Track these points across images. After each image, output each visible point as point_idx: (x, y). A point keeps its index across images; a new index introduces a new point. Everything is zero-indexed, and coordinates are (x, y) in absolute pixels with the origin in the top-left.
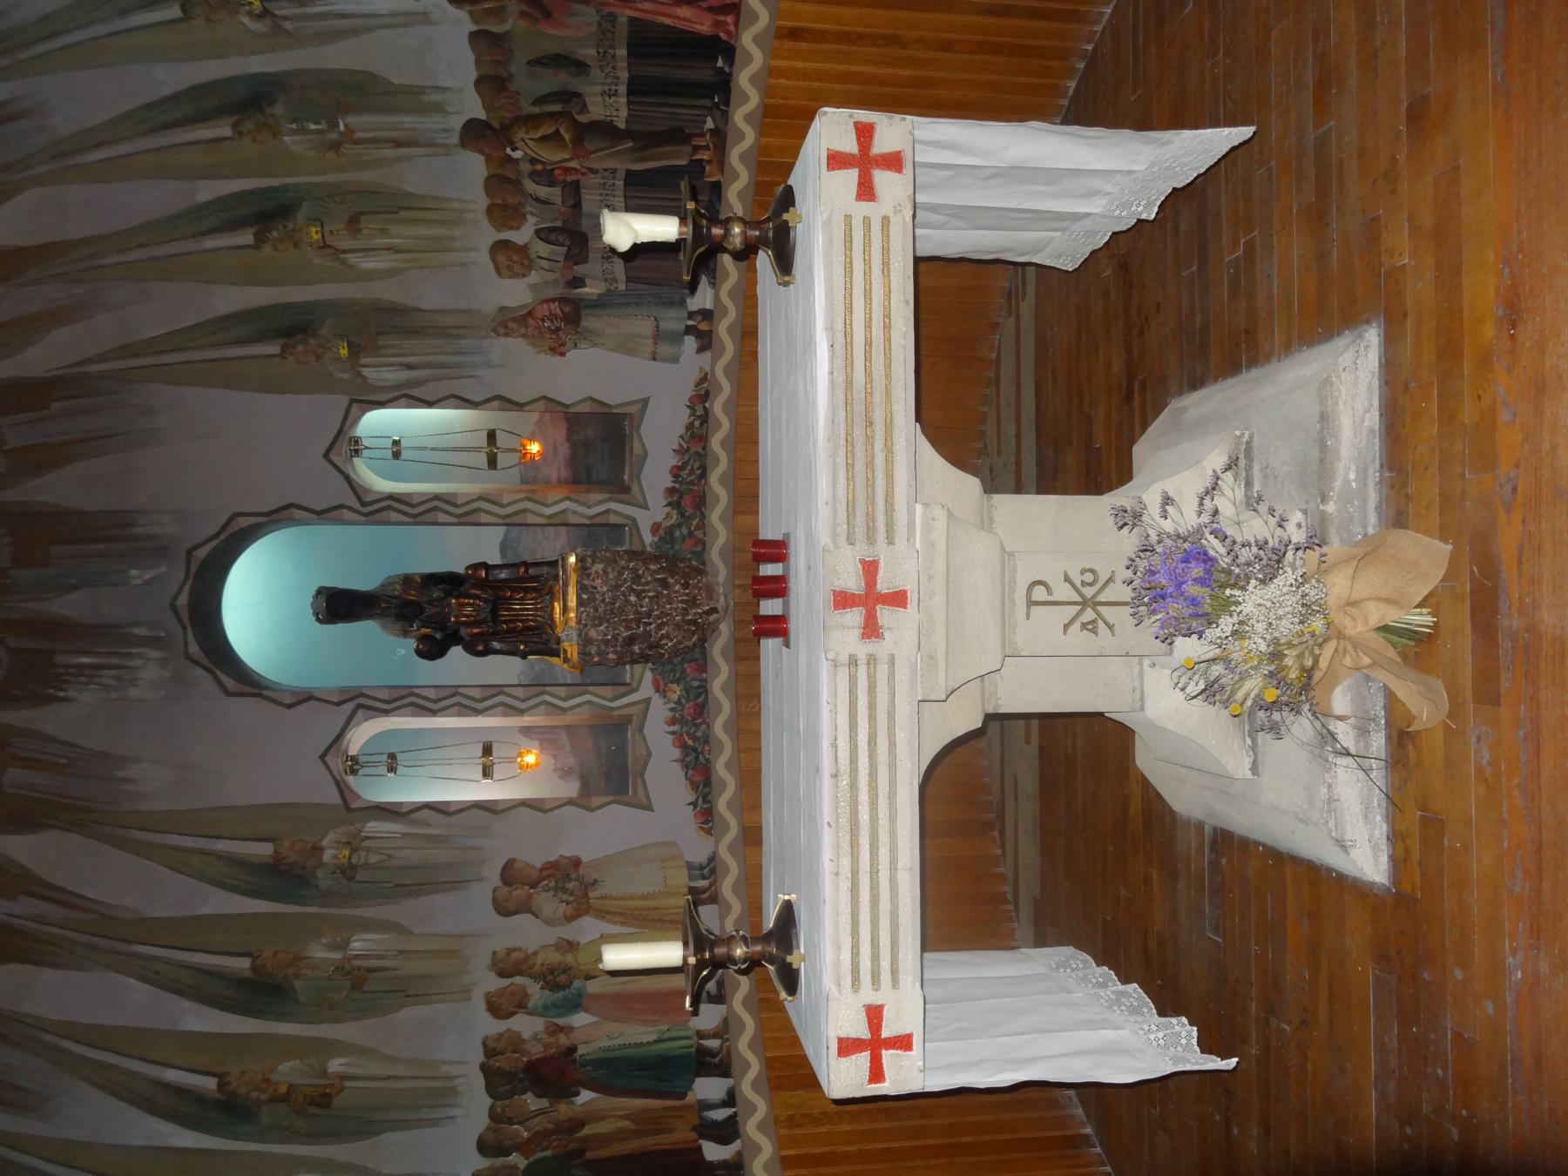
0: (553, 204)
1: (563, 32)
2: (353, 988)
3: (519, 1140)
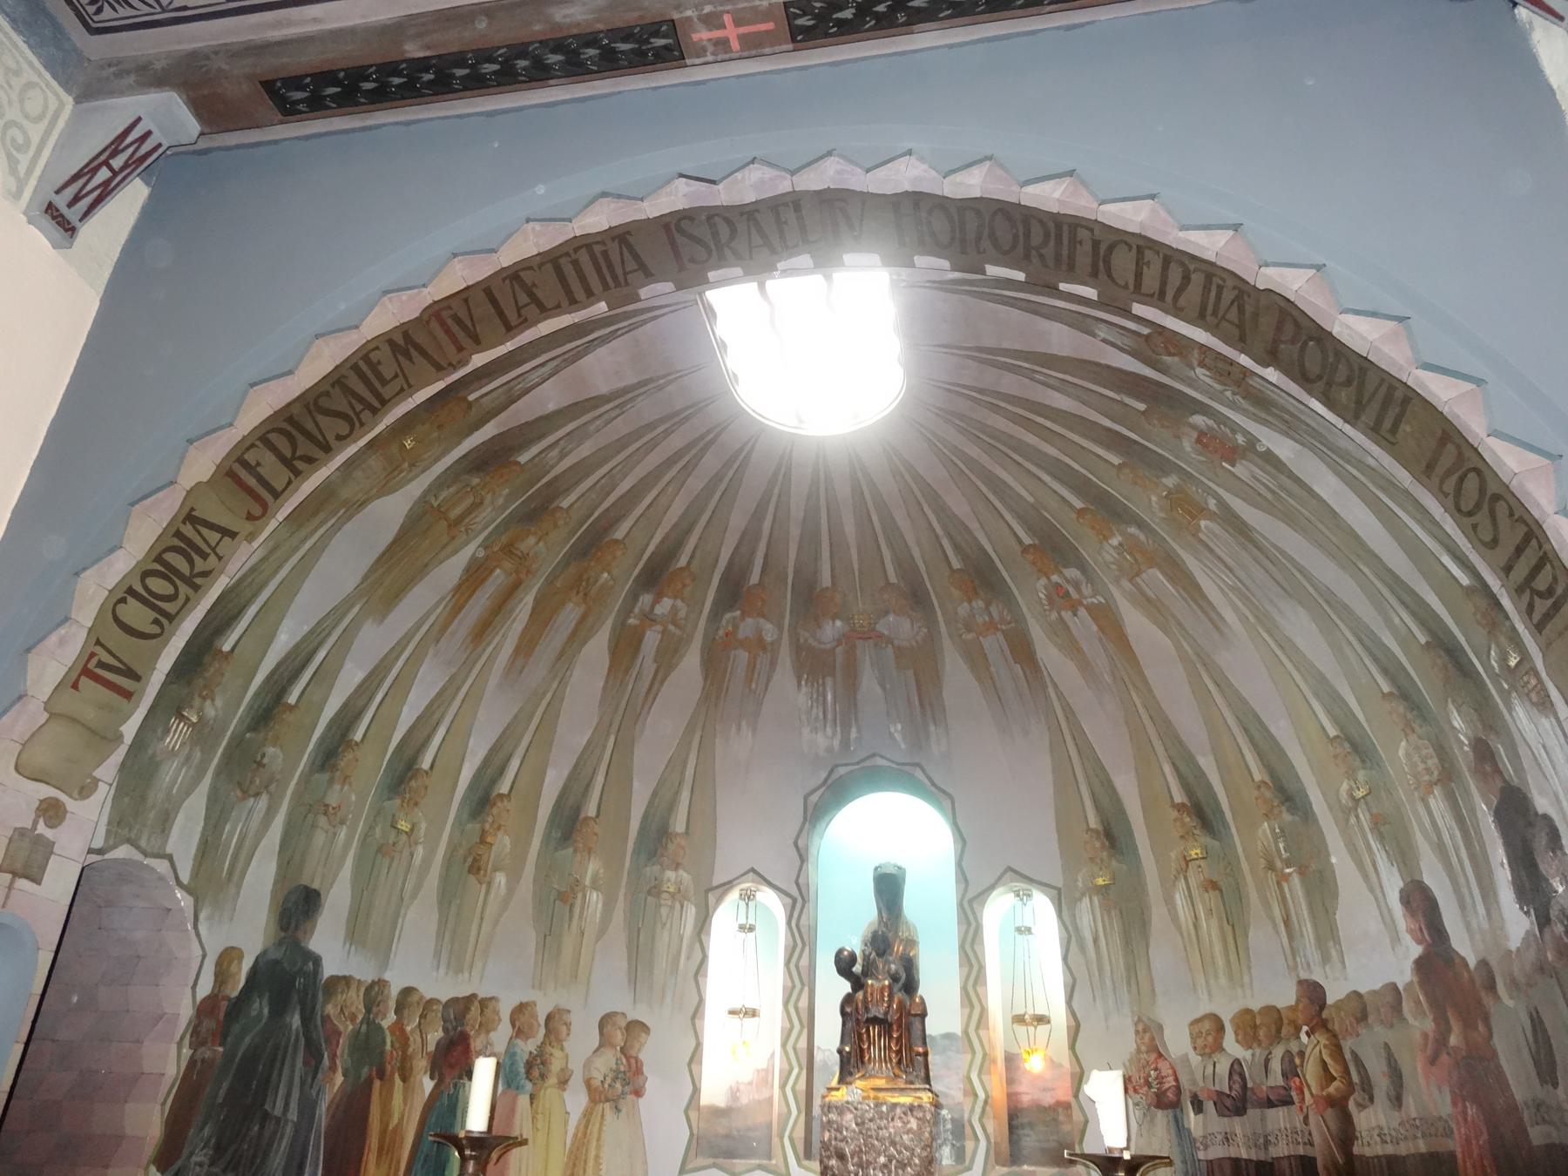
1: (1422, 1080)
2: (559, 892)
3: (405, 1022)
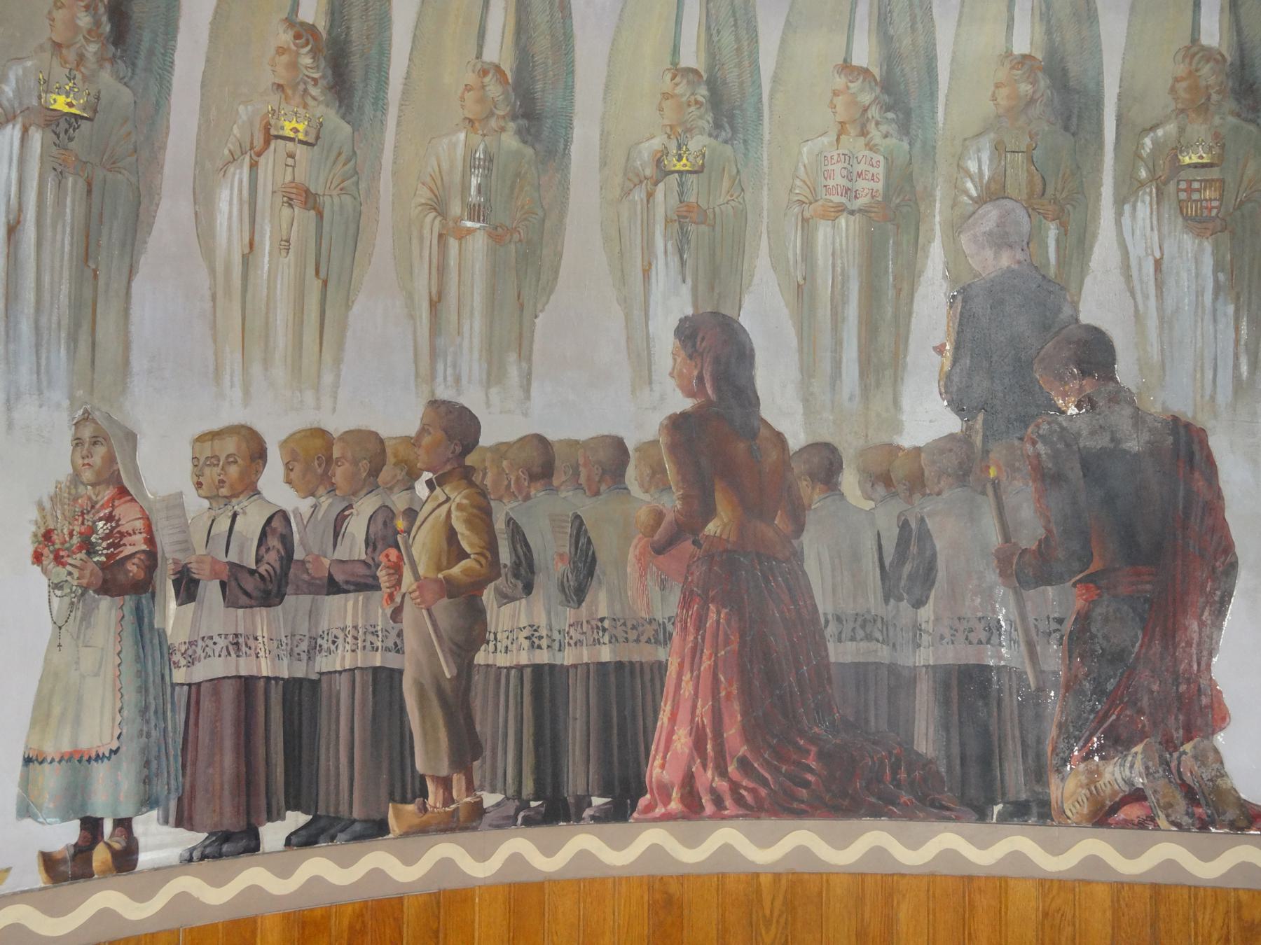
0: (335, 545)
1: (632, 569)
